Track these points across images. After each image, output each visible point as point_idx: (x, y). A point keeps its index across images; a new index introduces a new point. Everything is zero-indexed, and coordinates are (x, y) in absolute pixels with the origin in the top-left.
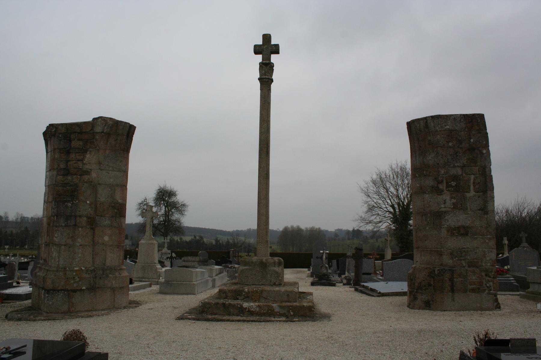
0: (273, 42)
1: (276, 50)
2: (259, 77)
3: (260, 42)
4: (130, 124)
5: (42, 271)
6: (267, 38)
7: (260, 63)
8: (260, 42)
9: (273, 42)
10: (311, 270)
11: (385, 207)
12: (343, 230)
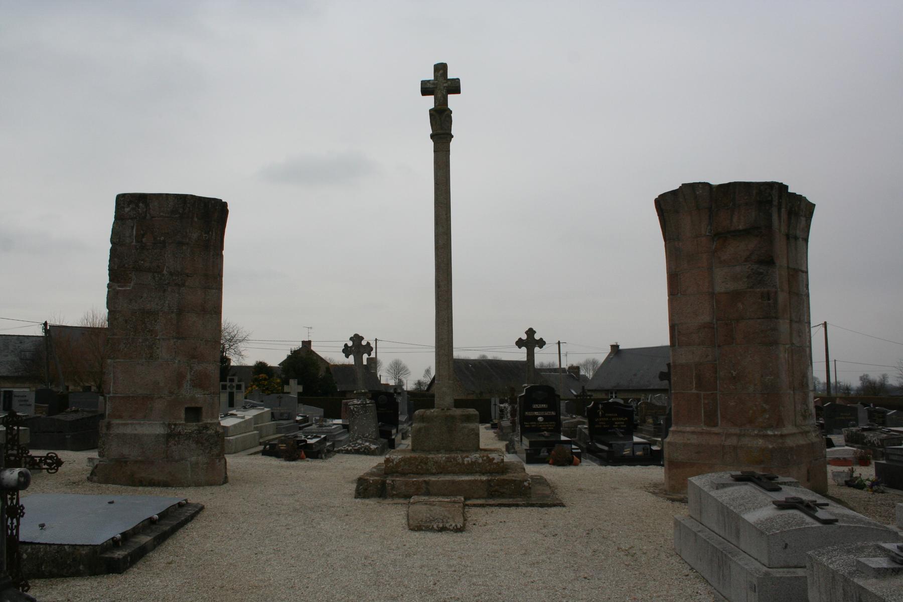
0: (451, 75)
1: (455, 87)
2: (431, 132)
3: (430, 76)
4: (108, 282)
5: (856, 482)
6: (441, 69)
7: (430, 111)
8: (430, 76)
9: (451, 75)
10: (586, 409)
11: (406, 446)
12: (790, 190)
